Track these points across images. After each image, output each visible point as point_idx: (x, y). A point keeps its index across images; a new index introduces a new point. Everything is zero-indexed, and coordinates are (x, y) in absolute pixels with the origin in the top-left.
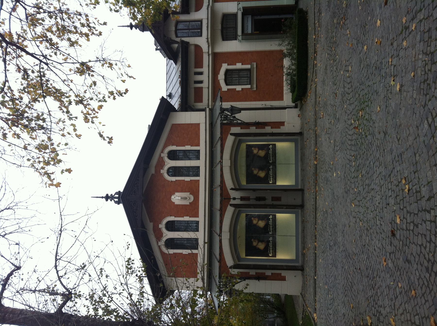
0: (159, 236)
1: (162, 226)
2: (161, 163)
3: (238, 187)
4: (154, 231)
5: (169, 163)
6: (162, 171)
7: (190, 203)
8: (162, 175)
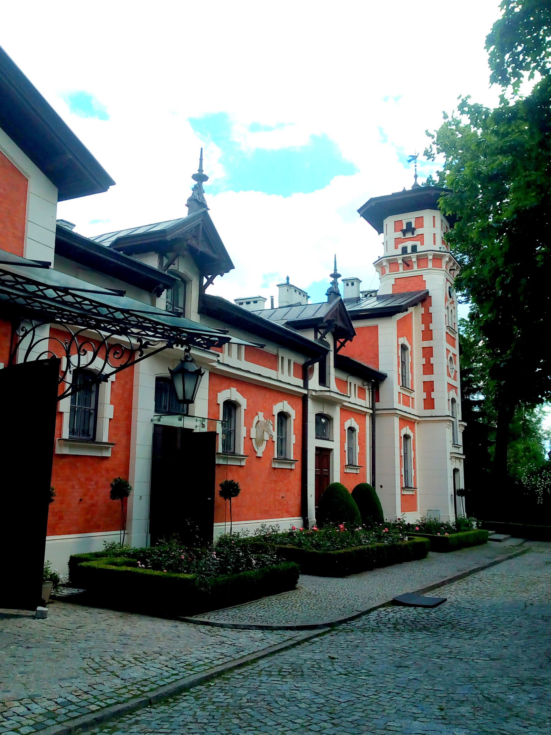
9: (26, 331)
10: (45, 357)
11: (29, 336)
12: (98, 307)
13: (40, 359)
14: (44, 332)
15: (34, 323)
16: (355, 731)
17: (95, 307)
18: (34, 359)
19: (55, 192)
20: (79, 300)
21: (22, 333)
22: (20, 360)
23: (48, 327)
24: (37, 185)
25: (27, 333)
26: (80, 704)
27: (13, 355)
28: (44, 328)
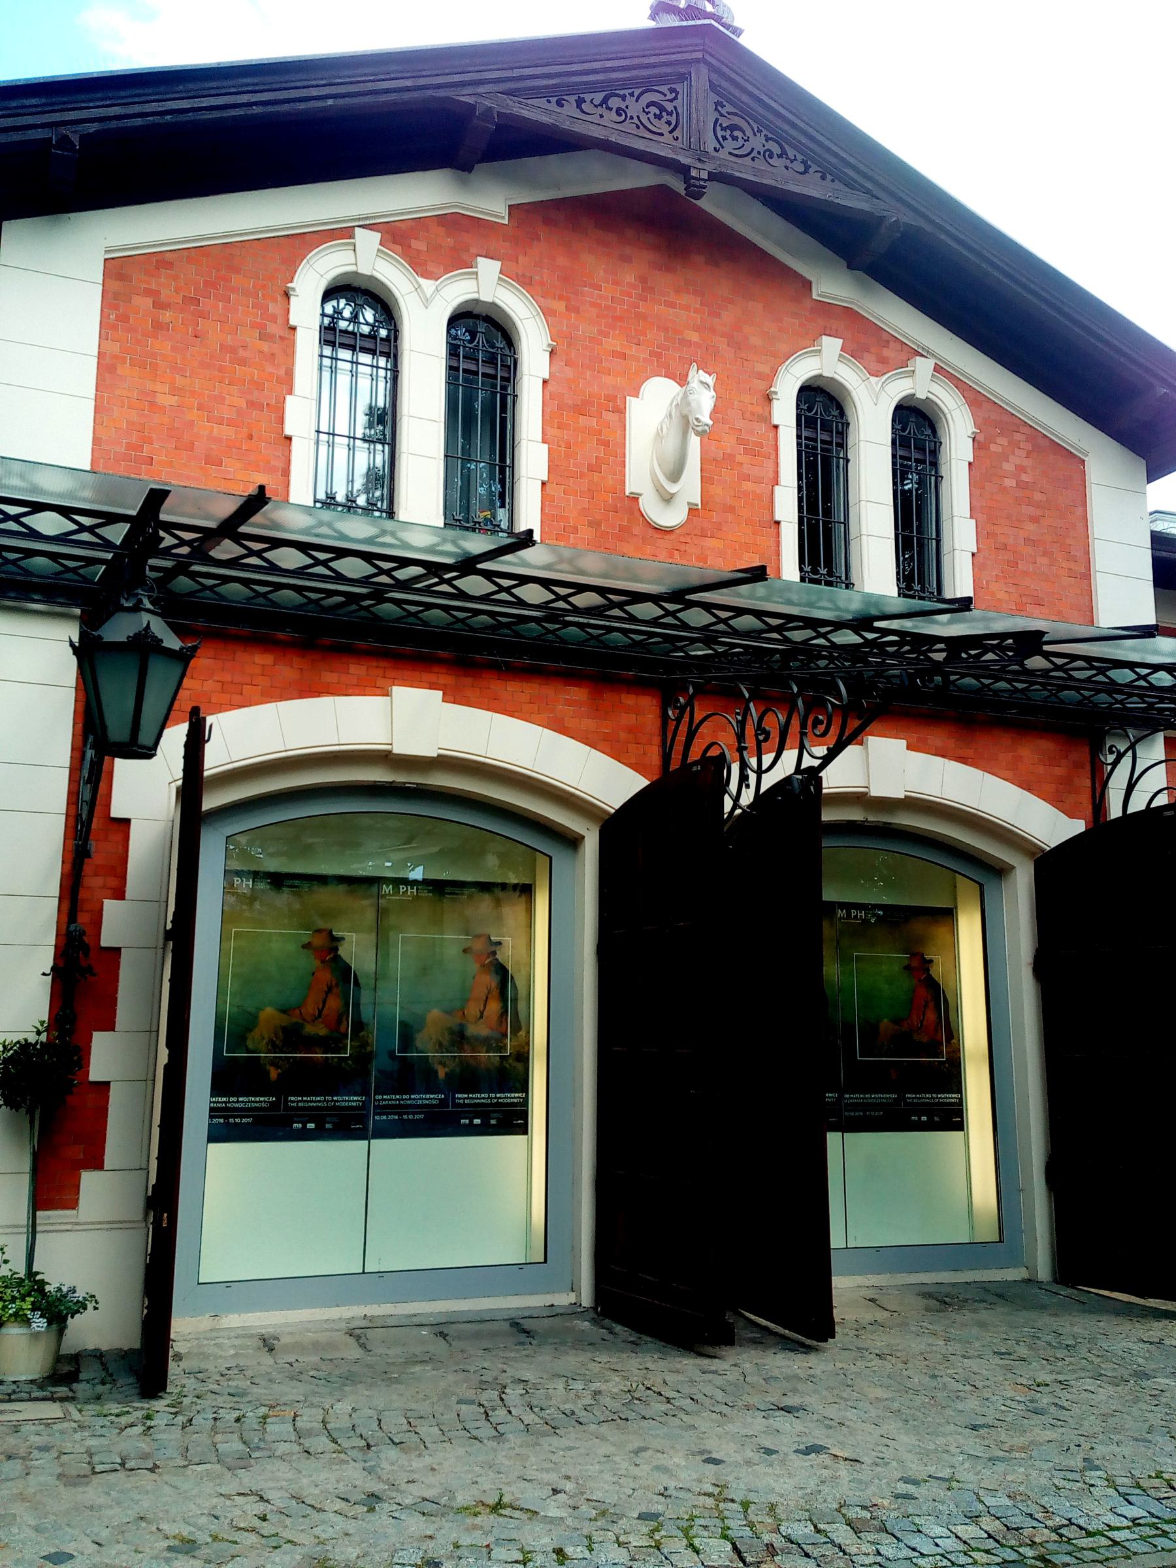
0: (432, 244)
1: (486, 282)
2: (875, 348)
3: (210, 802)
4: (453, 223)
5: (426, 302)
6: (488, 268)
7: (635, 499)
8: (806, 341)
9: (1118, 752)
10: (1162, 800)
11: (1127, 761)
12: (1109, 669)
13: (1153, 805)
14: (1155, 750)
15: (1131, 733)
16: (962, 1560)
17: (1102, 671)
18: (1142, 807)
19: (1141, 466)
20: (1059, 661)
21: (1111, 758)
22: (1115, 812)
23: (1160, 738)
24: (1103, 463)
25: (1120, 756)
26: (1155, 1532)
27: (1099, 804)
28: (1153, 740)
